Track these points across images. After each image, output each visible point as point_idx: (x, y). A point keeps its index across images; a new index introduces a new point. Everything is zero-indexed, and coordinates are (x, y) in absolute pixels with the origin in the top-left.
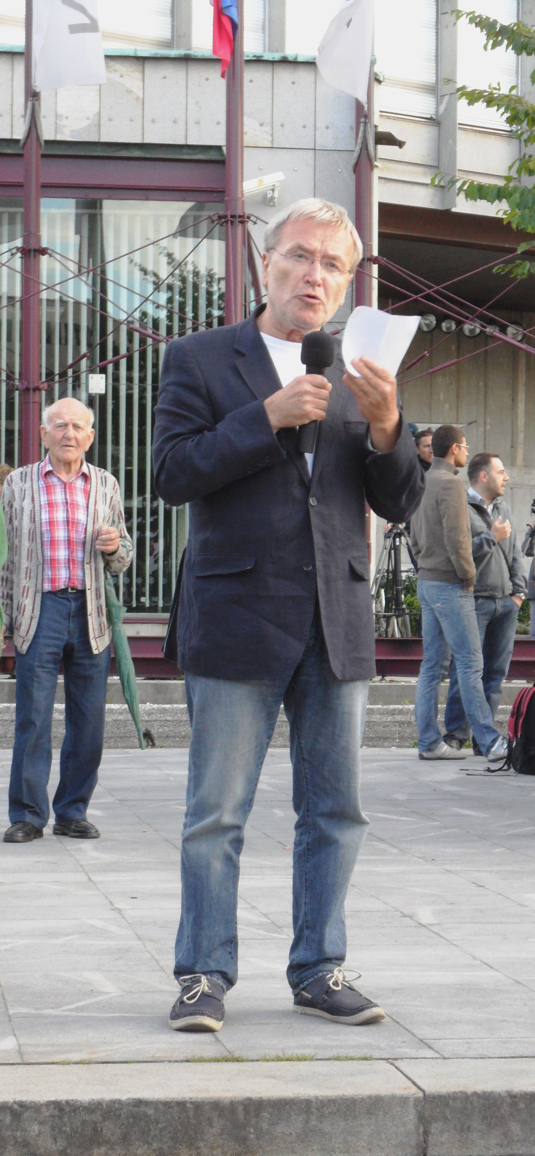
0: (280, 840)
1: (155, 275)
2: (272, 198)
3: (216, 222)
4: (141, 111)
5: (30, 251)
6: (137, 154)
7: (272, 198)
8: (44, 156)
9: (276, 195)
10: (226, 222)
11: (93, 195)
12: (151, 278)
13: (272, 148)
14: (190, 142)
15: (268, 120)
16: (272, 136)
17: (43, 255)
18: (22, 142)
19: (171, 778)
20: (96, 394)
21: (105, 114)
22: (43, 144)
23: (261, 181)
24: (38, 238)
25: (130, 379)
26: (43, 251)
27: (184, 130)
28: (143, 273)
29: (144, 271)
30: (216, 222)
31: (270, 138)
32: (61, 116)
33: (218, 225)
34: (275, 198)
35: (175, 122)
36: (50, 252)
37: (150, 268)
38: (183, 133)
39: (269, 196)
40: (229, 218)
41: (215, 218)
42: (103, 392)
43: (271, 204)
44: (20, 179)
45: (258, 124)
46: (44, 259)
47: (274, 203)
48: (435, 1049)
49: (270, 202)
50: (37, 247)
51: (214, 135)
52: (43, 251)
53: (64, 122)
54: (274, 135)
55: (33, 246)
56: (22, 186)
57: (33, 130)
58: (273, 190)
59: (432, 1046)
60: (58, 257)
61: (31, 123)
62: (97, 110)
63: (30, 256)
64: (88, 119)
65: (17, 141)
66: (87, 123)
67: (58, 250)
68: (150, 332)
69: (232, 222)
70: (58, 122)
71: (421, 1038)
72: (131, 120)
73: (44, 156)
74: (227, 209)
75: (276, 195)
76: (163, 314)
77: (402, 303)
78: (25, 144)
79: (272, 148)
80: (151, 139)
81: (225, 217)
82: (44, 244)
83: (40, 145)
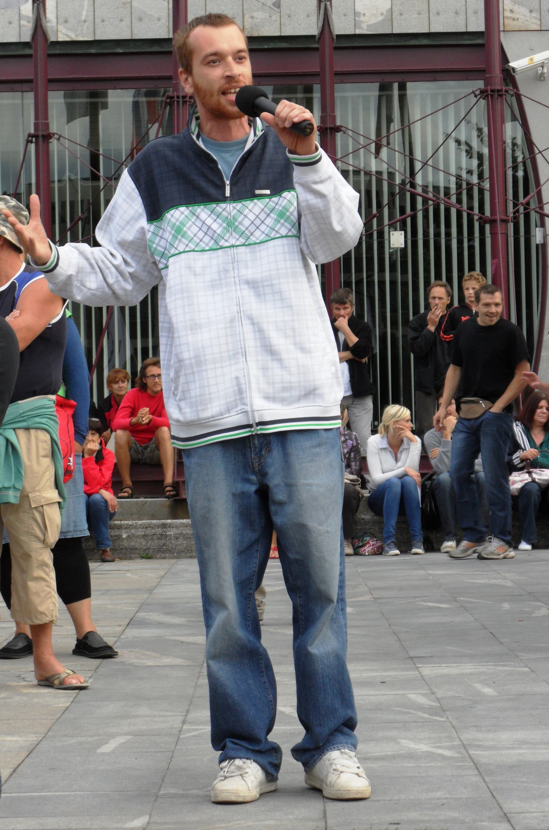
0: (492, 631)
1: (467, 144)
2: (542, 74)
3: (479, 97)
4: (427, 5)
5: (326, 129)
6: (425, 42)
7: (542, 74)
8: (336, 48)
9: (545, 70)
10: (487, 96)
11: (94, 87)
12: (464, 147)
13: (541, 30)
14: (470, 29)
15: (537, 7)
16: (540, 20)
17: (338, 132)
18: (317, 37)
19: (431, 577)
20: (397, 248)
21: (395, 9)
22: (335, 37)
23: (532, 59)
24: (334, 118)
25: (448, 235)
26: (338, 129)
27: (464, 20)
28: (457, 144)
29: (458, 142)
30: (479, 97)
31: (539, 22)
32: (359, 13)
33: (481, 99)
34: (544, 73)
35: (456, 13)
36: (343, 129)
37: (463, 139)
38: (464, 22)
39: (540, 72)
40: (489, 93)
41: (478, 92)
42: (403, 246)
43: (542, 79)
44: (31, 77)
45: (528, 11)
46: (339, 135)
47: (544, 78)
48: (512, 822)
49: (540, 77)
50: (332, 126)
51: (477, 24)
52: (338, 129)
53: (362, 18)
54: (543, 21)
55: (329, 125)
56: (318, 75)
57: (326, 26)
58: (543, 67)
59: (510, 820)
60: (350, 133)
61: (324, 20)
62: (388, 6)
63: (327, 134)
64: (382, 14)
65: (313, 37)
66: (380, 18)
67: (350, 128)
68: (431, 195)
69: (492, 96)
70: (356, 18)
71: (505, 811)
72: (419, 14)
73: (336, 48)
74: (486, 85)
75: (545, 70)
76: (475, 179)
77: (79, 168)
78: (319, 39)
79: (541, 30)
80: (437, 28)
81: (487, 91)
82: (338, 123)
83: (333, 39)
